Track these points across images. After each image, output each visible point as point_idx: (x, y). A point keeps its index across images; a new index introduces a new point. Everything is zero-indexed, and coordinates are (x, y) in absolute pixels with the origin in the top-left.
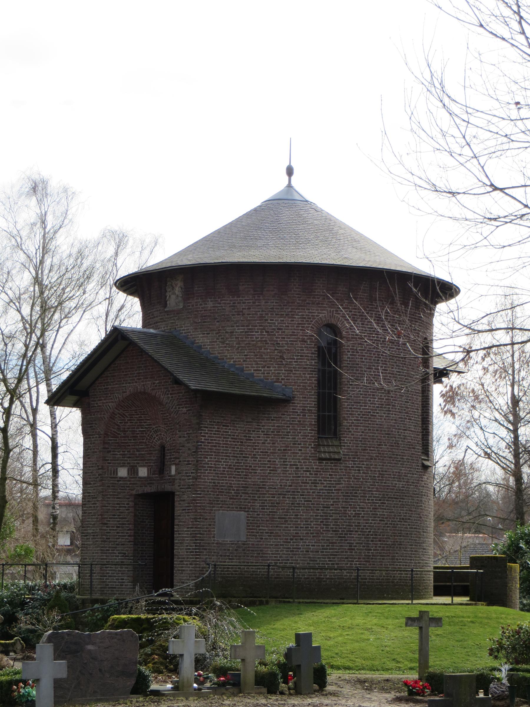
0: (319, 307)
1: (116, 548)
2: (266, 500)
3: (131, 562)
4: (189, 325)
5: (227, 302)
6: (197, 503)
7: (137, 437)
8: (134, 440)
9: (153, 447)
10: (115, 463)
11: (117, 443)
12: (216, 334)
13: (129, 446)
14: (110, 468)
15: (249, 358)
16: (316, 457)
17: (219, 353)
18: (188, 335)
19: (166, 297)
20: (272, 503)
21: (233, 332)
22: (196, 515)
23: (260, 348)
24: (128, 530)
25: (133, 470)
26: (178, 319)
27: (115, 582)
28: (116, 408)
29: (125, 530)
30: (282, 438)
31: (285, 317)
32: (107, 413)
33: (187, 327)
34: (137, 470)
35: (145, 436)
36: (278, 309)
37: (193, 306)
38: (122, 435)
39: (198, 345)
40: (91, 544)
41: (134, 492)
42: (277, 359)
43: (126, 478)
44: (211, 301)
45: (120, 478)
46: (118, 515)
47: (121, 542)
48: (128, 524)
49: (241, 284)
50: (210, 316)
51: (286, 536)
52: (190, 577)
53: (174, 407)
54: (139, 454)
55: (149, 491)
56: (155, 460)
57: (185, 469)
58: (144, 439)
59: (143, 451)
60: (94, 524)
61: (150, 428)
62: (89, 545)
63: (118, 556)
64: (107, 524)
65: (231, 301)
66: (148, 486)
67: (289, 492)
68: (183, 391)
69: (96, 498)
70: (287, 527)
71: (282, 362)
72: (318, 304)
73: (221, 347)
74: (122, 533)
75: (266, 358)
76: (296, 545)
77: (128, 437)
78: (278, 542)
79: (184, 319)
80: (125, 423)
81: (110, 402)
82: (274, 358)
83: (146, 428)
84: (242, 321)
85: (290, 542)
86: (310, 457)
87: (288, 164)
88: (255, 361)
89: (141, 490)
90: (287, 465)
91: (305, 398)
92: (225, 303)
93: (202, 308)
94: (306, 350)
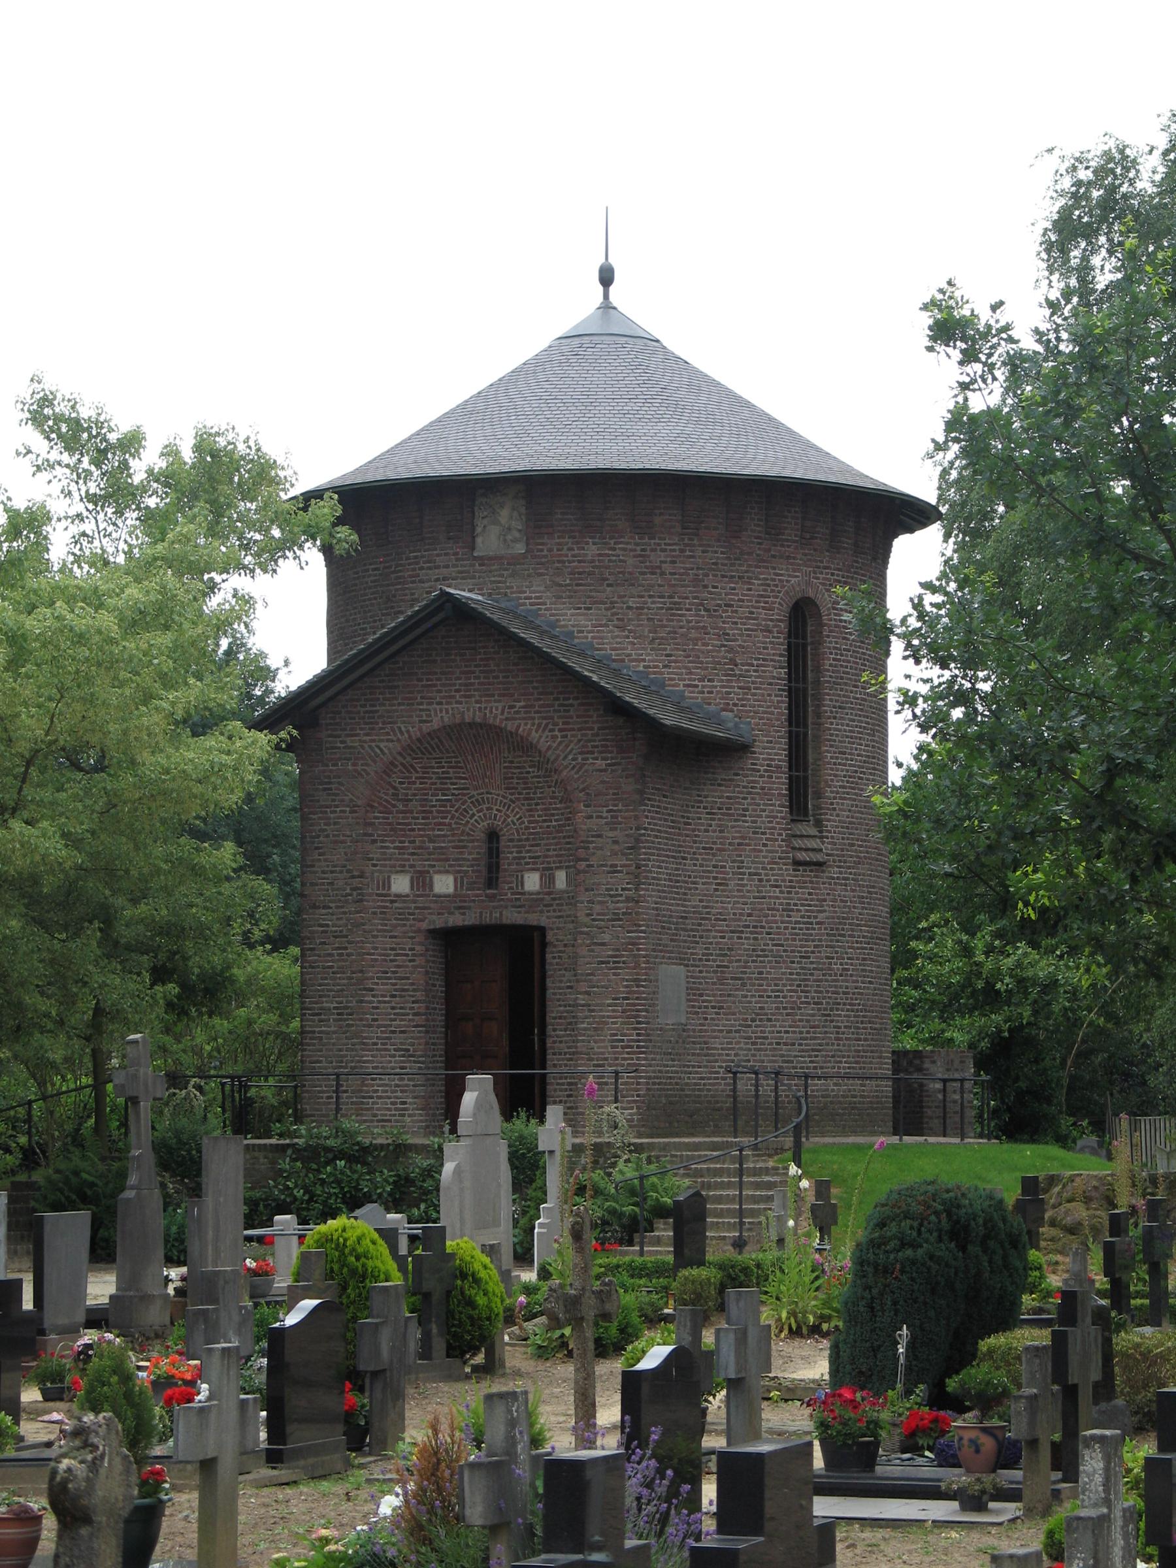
0: (792, 564)
2: (711, 943)
3: (420, 1068)
4: (542, 589)
5: (629, 547)
6: (639, 950)
7: (431, 812)
8: (423, 818)
9: (468, 834)
10: (385, 866)
11: (389, 824)
12: (607, 609)
13: (413, 830)
14: (376, 874)
15: (676, 662)
16: (788, 858)
17: (613, 649)
18: (540, 609)
19: (473, 530)
20: (720, 949)
21: (642, 608)
22: (638, 974)
23: (695, 641)
25: (422, 881)
26: (512, 575)
27: (389, 1109)
28: (400, 754)
30: (736, 821)
31: (737, 583)
32: (375, 762)
33: (534, 592)
35: (449, 812)
36: (725, 565)
37: (550, 550)
39: (565, 629)
40: (334, 1032)
41: (424, 926)
42: (725, 664)
43: (407, 896)
44: (594, 544)
45: (396, 895)
46: (394, 972)
47: (399, 1026)
49: (657, 511)
51: (745, 1014)
53: (570, 757)
54: (434, 848)
55: (460, 923)
56: (474, 859)
57: (604, 881)
58: (446, 818)
59: (444, 842)
60: (342, 990)
61: (464, 795)
62: (327, 1033)
63: (394, 1056)
64: (372, 990)
65: (637, 544)
66: (457, 912)
67: (748, 926)
68: (596, 726)
69: (346, 936)
70: (746, 996)
71: (732, 670)
72: (788, 557)
73: (617, 637)
74: (401, 1008)
75: (707, 663)
76: (762, 1032)
77: (412, 812)
78: (732, 1025)
79: (529, 576)
80: (409, 783)
81: (382, 741)
82: (719, 663)
83: (453, 794)
84: (659, 586)
85: (750, 1026)
86: (780, 858)
88: (686, 668)
89: (439, 923)
90: (744, 874)
91: (771, 742)
92: (624, 549)
93: (573, 556)
94: (773, 649)
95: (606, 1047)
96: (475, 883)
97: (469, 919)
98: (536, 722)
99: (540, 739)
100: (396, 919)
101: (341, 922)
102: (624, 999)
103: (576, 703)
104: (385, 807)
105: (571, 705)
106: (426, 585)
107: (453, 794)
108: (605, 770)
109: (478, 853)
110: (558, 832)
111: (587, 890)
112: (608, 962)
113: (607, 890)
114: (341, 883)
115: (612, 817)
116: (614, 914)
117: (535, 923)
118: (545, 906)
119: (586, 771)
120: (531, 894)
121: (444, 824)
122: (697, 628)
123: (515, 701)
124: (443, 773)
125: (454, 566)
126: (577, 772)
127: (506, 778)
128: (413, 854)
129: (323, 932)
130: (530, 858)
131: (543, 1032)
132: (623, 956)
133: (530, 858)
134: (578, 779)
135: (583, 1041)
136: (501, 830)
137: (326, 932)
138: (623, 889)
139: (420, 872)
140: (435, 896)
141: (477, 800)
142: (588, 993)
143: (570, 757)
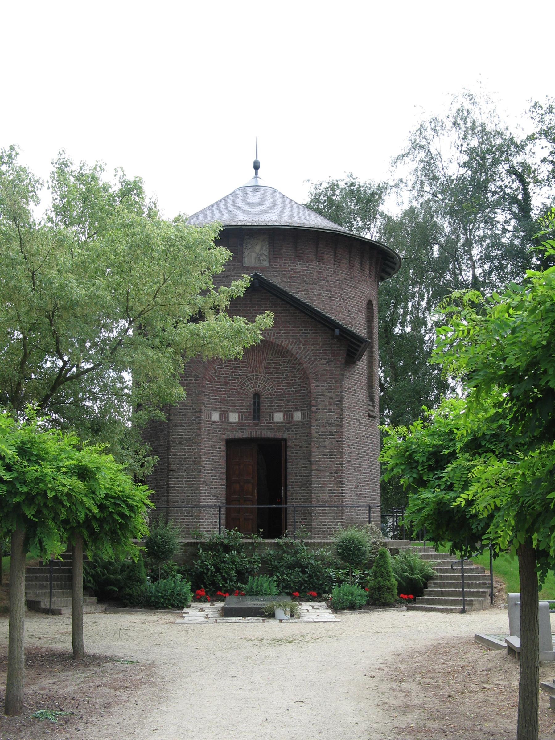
1: (210, 491)
5: (315, 267)
7: (229, 383)
8: (226, 386)
9: (245, 394)
13: (221, 391)
21: (319, 295)
24: (220, 474)
27: (210, 525)
29: (217, 473)
34: (228, 414)
35: (237, 383)
37: (280, 265)
38: (217, 380)
40: (185, 487)
41: (225, 437)
43: (218, 422)
45: (214, 422)
47: (214, 485)
48: (221, 468)
50: (298, 277)
52: (335, 519)
53: (308, 357)
55: (241, 436)
56: (247, 406)
57: (325, 417)
60: (190, 467)
61: (245, 375)
65: (318, 266)
68: (321, 343)
69: (192, 440)
74: (215, 476)
80: (222, 368)
83: (239, 375)
84: (327, 286)
87: (255, 159)
89: (231, 435)
92: (313, 268)
93: (291, 269)
95: (326, 496)
96: (248, 417)
97: (245, 434)
98: (291, 340)
99: (293, 349)
100: (214, 433)
101: (189, 434)
102: (335, 473)
103: (310, 332)
104: (210, 379)
105: (309, 333)
106: (218, 279)
107: (239, 375)
108: (326, 364)
109: (250, 404)
110: (295, 394)
111: (316, 420)
112: (327, 455)
113: (327, 421)
114: (190, 414)
115: (329, 386)
116: (330, 432)
117: (280, 437)
118: (287, 429)
119: (316, 364)
120: (277, 423)
121: (234, 389)
122: (340, 307)
123: (280, 330)
124: (237, 364)
125: (233, 271)
126: (312, 364)
127: (267, 368)
128: (221, 402)
129: (180, 438)
130: (277, 406)
131: (286, 489)
132: (335, 452)
133: (277, 406)
134: (312, 368)
135: (315, 493)
136: (262, 392)
137: (182, 438)
138: (334, 421)
139: (224, 411)
140: (229, 423)
141: (250, 378)
142: (317, 470)
143: (308, 357)
